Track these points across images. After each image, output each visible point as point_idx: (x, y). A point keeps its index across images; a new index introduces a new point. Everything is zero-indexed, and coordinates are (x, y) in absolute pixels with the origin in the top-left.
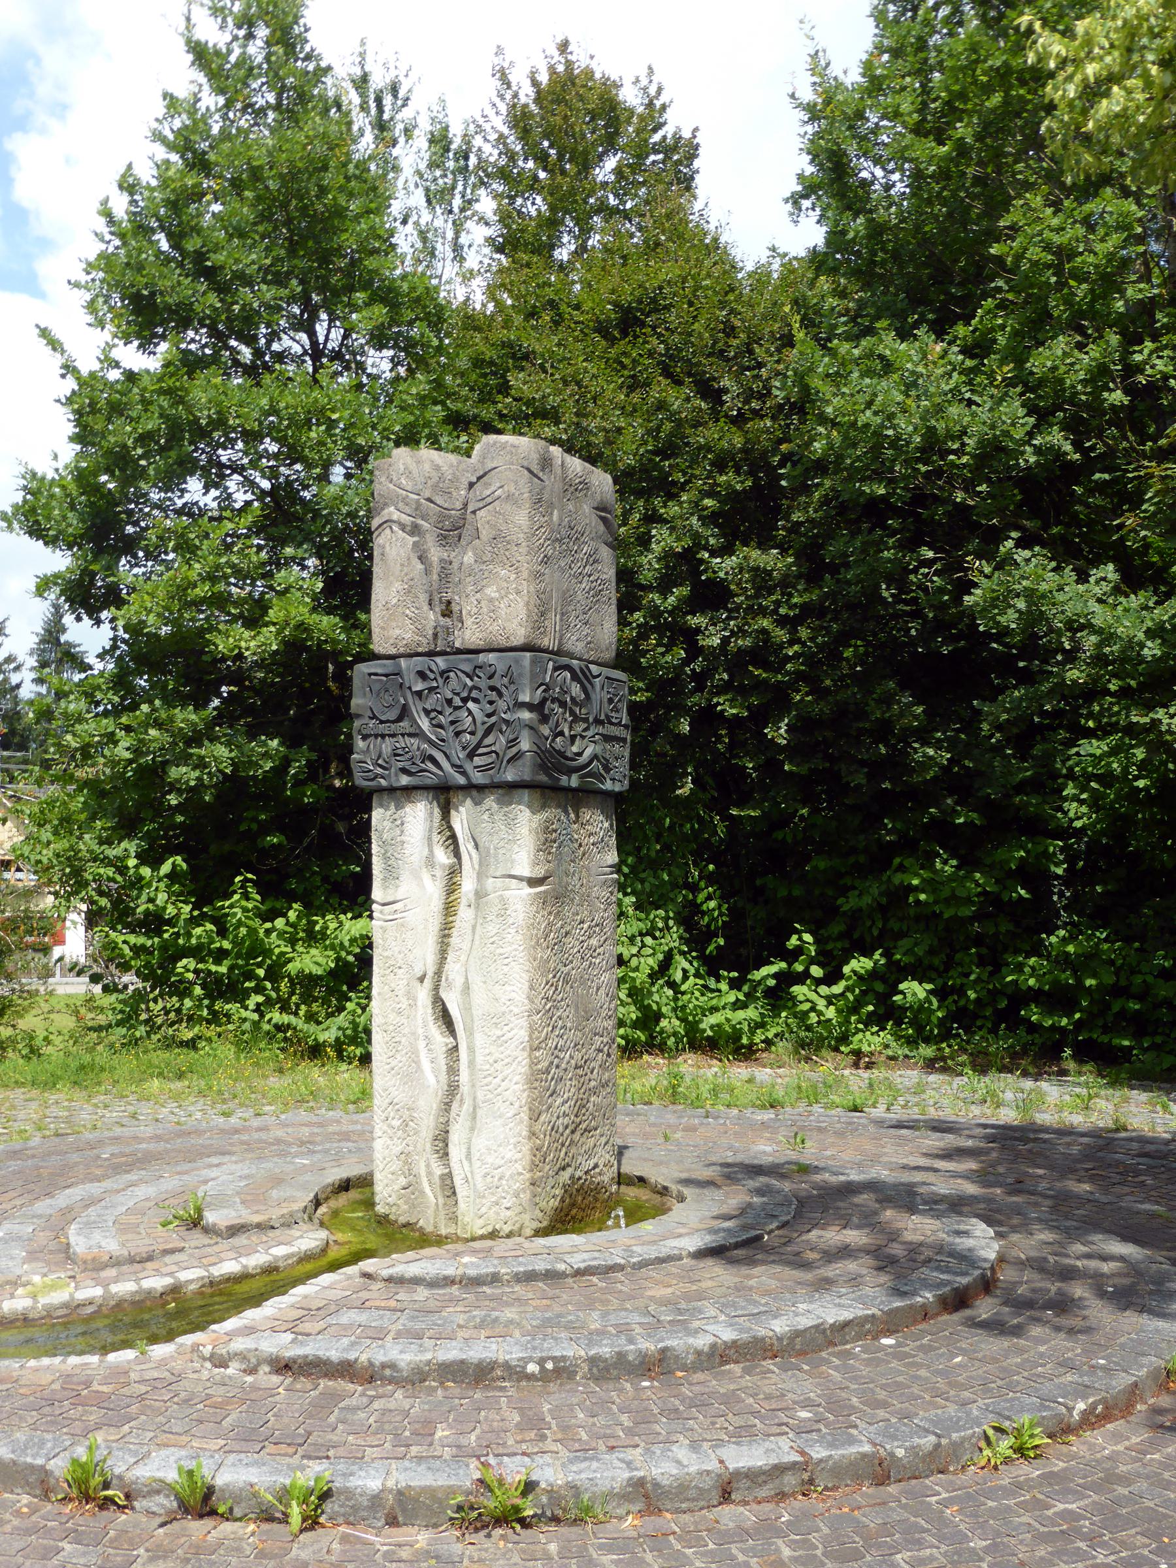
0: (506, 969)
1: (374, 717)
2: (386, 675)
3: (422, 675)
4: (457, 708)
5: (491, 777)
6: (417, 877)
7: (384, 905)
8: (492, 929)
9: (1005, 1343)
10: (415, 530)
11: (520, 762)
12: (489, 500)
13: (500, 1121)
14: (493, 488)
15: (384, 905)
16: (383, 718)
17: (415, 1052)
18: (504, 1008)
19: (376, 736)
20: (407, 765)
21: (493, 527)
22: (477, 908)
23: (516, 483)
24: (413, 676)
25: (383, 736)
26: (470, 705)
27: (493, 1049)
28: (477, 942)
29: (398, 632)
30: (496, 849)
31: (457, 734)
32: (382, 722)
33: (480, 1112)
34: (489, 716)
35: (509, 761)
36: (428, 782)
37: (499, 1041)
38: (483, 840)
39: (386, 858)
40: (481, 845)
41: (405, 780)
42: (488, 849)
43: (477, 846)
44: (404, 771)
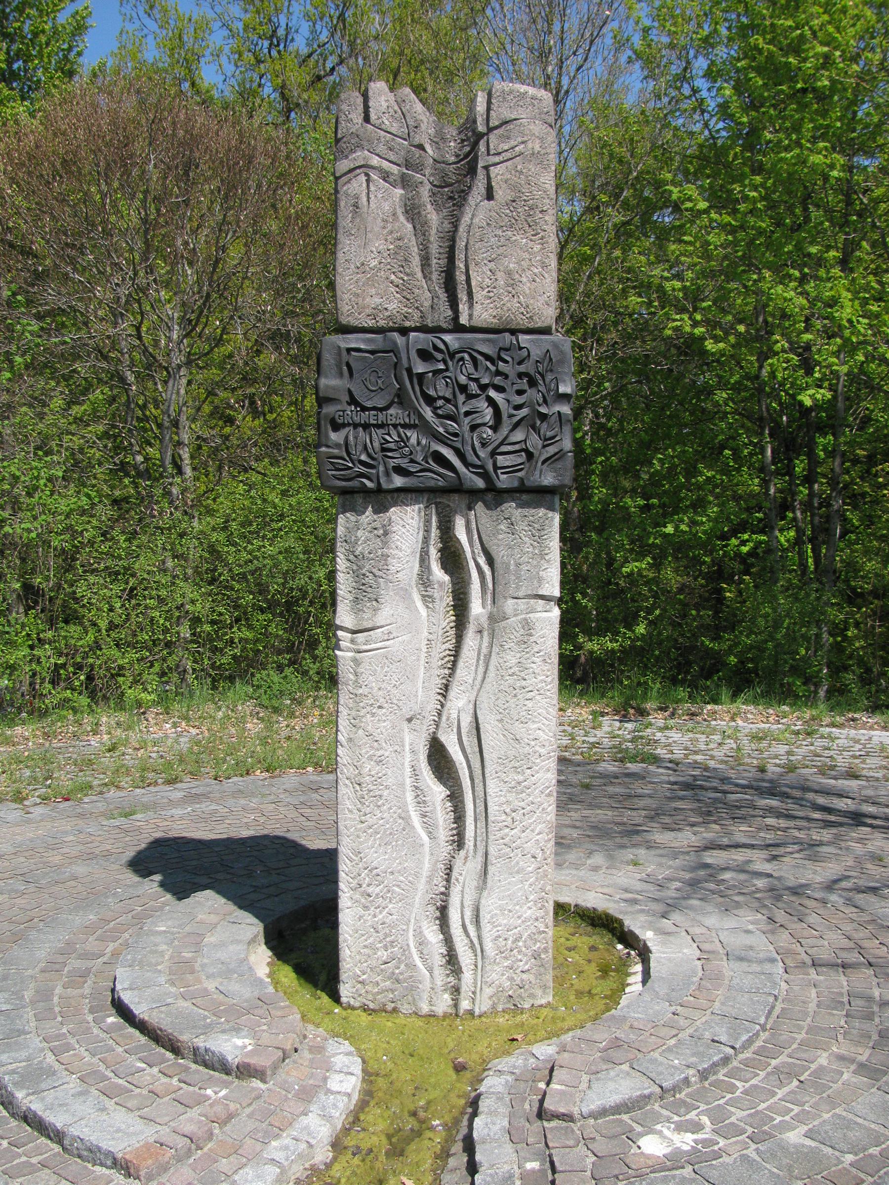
0: (530, 704)
1: (353, 401)
2: (372, 352)
3: (424, 355)
4: (471, 397)
5: (521, 480)
6: (405, 595)
7: (354, 632)
8: (511, 659)
9: (672, 834)
10: (404, 182)
11: (559, 465)
12: (508, 155)
13: (518, 877)
14: (513, 143)
15: (354, 632)
16: (368, 404)
17: (404, 807)
18: (527, 749)
19: (356, 426)
20: (404, 463)
21: (515, 188)
22: (492, 635)
23: (542, 139)
24: (413, 354)
25: (366, 426)
26: (492, 393)
27: (511, 797)
28: (492, 673)
29: (378, 300)
30: (518, 565)
31: (473, 428)
32: (364, 409)
33: (491, 869)
34: (518, 407)
35: (544, 462)
36: (432, 483)
37: (518, 788)
38: (500, 554)
39: (358, 575)
40: (498, 560)
41: (398, 481)
42: (508, 565)
43: (491, 561)
44: (400, 471)
